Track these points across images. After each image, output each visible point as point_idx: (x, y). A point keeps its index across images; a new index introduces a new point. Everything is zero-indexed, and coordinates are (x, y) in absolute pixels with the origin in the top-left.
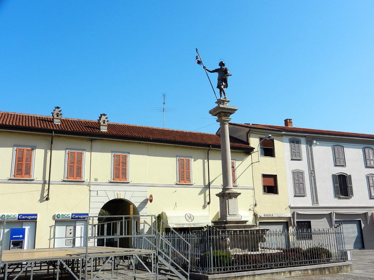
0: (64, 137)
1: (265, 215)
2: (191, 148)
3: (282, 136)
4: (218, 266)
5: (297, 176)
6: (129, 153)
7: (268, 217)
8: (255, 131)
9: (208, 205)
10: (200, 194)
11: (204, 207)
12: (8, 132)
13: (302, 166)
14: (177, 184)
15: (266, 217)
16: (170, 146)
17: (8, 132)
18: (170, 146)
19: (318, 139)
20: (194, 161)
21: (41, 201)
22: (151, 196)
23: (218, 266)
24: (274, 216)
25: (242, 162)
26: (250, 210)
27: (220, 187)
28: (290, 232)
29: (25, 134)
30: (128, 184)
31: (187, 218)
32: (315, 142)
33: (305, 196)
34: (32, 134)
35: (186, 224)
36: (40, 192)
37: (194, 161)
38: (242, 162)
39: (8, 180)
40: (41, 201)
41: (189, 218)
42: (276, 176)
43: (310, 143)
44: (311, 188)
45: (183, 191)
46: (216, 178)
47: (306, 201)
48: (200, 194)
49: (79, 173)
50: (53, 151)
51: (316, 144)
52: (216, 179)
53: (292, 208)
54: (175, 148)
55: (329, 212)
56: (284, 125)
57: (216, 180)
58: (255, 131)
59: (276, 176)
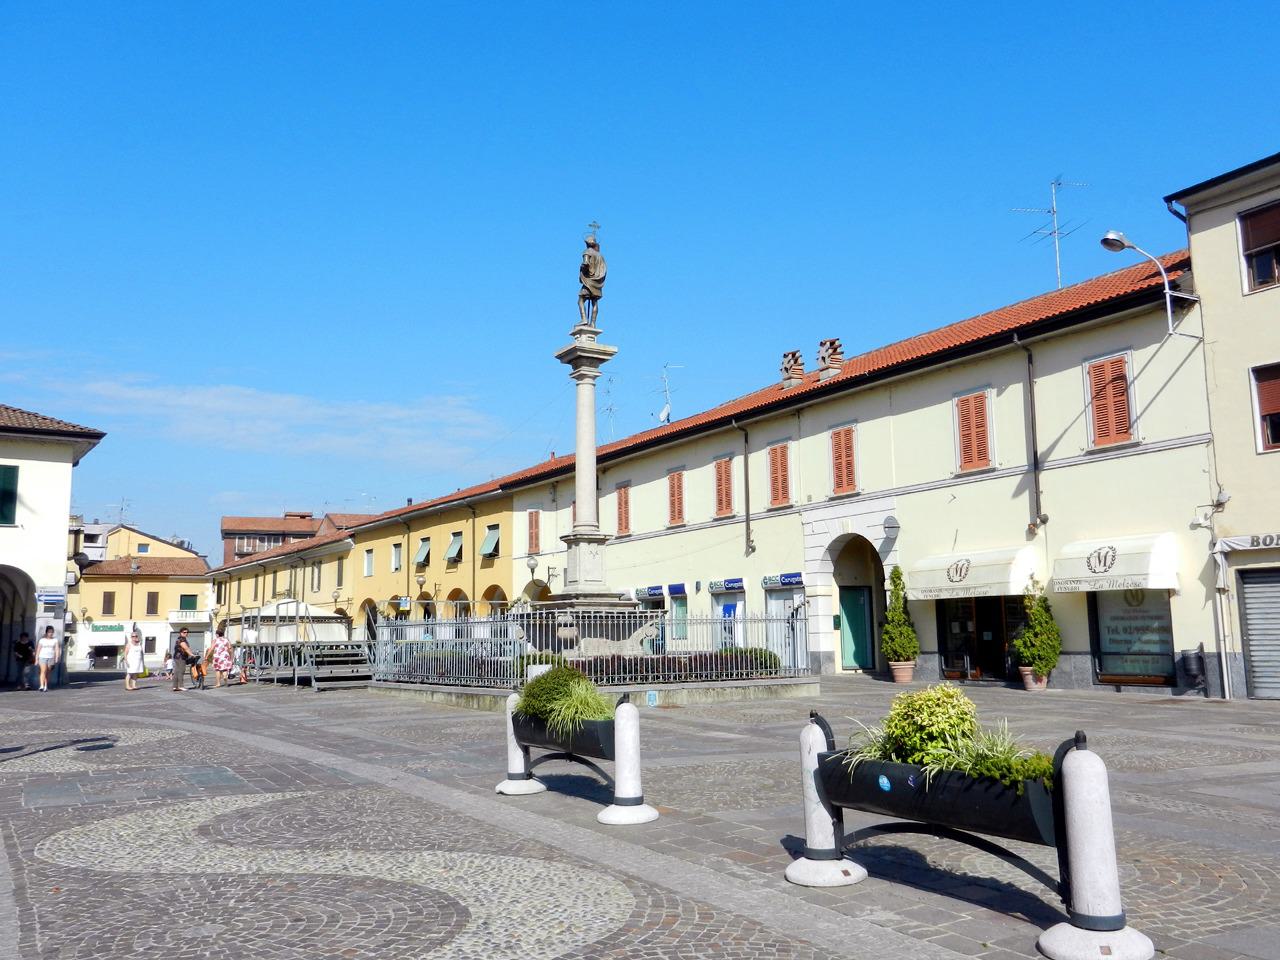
0: (714, 434)
2: (991, 357)
4: (630, 672)
6: (856, 421)
7: (1273, 546)
8: (1215, 197)
9: (1043, 526)
10: (1018, 493)
11: (1031, 532)
12: (940, 369)
14: (716, 520)
15: (1262, 546)
16: (932, 372)
17: (940, 369)
18: (932, 372)
20: (999, 394)
21: (748, 554)
23: (630, 672)
25: (1161, 347)
26: (1195, 526)
27: (1079, 458)
28: (689, 617)
29: (962, 364)
30: (1138, 449)
31: (1095, 561)
35: (946, 590)
36: (745, 536)
37: (999, 394)
38: (1161, 347)
39: (953, 478)
40: (748, 554)
41: (1100, 562)
42: (182, 596)
45: (974, 491)
46: (1066, 430)
48: (1018, 493)
49: (983, 454)
52: (1061, 436)
54: (950, 371)
57: (1065, 437)
58: (1215, 197)
59: (182, 596)
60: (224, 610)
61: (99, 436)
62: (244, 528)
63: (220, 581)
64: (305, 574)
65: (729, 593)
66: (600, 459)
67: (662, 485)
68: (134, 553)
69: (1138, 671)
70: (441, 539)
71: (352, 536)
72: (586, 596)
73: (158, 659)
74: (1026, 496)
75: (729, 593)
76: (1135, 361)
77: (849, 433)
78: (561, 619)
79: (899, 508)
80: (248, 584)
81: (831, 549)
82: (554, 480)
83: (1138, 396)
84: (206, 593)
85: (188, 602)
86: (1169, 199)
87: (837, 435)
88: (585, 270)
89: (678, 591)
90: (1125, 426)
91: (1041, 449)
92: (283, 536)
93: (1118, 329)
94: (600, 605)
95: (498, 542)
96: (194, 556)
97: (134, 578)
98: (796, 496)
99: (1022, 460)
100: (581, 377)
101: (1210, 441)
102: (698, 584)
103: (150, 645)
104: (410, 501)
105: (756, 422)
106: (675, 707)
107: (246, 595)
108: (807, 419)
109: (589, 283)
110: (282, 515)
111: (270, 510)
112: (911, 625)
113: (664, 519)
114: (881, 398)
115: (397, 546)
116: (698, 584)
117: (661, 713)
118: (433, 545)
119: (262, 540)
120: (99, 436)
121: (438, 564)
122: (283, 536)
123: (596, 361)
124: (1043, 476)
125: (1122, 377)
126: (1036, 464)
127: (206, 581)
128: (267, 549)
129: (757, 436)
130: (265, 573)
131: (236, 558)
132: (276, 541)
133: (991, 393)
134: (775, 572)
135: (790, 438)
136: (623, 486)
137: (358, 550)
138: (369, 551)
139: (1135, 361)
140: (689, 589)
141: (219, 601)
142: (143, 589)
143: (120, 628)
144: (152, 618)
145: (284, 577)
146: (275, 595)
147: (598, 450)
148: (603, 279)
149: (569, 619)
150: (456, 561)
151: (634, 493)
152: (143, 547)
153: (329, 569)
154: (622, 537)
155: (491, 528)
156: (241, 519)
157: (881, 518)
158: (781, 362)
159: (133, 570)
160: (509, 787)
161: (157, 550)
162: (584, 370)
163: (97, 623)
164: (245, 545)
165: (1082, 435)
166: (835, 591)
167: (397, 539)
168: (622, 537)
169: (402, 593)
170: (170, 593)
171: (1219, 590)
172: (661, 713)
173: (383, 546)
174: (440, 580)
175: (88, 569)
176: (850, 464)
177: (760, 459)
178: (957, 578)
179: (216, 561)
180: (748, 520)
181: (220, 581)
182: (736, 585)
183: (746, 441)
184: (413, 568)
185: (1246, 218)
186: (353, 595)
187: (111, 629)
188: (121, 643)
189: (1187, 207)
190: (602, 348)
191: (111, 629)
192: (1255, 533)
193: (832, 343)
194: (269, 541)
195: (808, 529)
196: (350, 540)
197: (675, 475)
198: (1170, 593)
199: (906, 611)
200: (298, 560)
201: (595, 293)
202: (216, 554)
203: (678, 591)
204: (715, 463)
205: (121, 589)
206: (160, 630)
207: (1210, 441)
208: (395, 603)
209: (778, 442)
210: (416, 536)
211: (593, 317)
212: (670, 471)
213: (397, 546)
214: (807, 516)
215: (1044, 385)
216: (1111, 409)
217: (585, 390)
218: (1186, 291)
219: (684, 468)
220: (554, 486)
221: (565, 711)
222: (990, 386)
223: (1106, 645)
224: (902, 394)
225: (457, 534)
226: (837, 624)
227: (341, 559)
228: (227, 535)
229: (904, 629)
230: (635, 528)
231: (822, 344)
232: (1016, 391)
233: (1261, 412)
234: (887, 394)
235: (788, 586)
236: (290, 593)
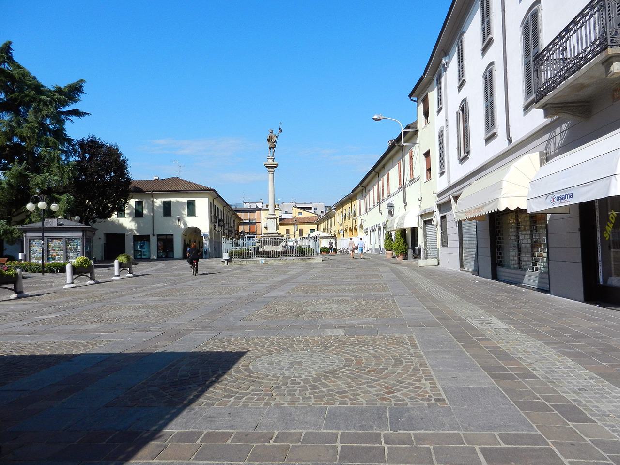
55: (446, 199)
88: (268, 140)
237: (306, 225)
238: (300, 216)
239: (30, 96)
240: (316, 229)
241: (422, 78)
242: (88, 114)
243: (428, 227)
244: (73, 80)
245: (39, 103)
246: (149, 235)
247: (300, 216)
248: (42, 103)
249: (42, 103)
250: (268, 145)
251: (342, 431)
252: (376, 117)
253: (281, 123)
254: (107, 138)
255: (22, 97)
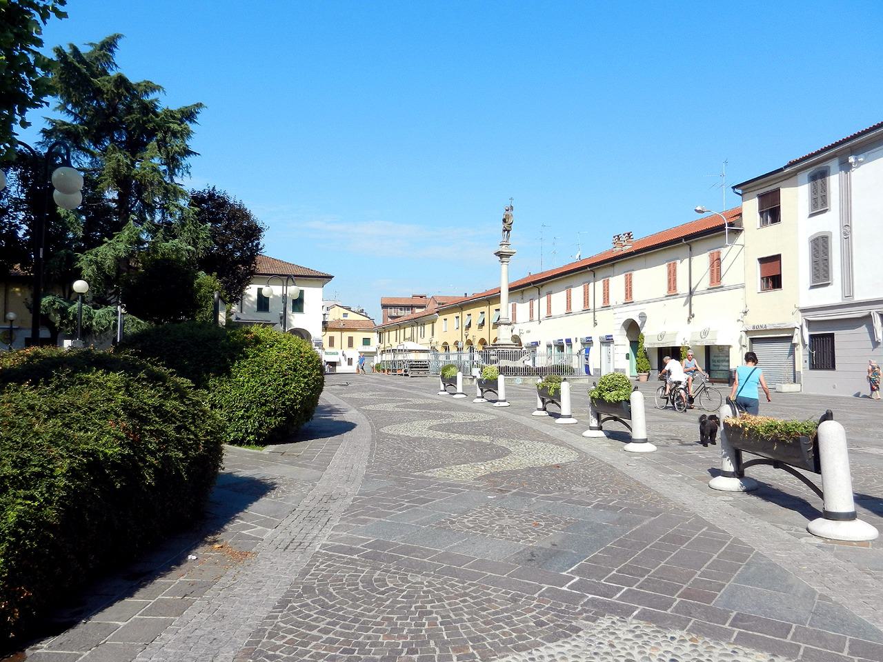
1: (754, 327)
3: (796, 175)
5: (820, 246)
10: (685, 305)
13: (828, 223)
19: (855, 151)
22: (29, 124)
24: (768, 328)
32: (852, 159)
33: (828, 284)
34: (673, 248)
43: (846, 167)
44: (843, 265)
47: (831, 295)
48: (685, 305)
50: (288, 287)
51: (859, 164)
53: (803, 311)
55: (865, 313)
56: (517, 304)
60: (382, 346)
61: (331, 277)
62: (392, 303)
63: (381, 331)
64: (417, 329)
65: (588, 343)
66: (510, 290)
67: (564, 294)
68: (342, 318)
69: (721, 377)
70: (476, 314)
71: (437, 312)
72: (502, 345)
73: (353, 369)
74: (688, 305)
75: (588, 343)
76: (724, 251)
77: (631, 275)
78: (492, 353)
79: (648, 309)
80: (393, 334)
81: (623, 325)
82: (491, 298)
83: (724, 266)
84: (374, 337)
85: (366, 342)
86: (734, 188)
87: (626, 275)
88: (504, 221)
89: (569, 341)
90: (719, 278)
91: (693, 287)
92: (411, 307)
93: (714, 240)
94: (507, 348)
95: (484, 320)
96: (368, 319)
97: (342, 330)
98: (612, 302)
99: (687, 291)
100: (503, 262)
101: (744, 287)
102: (576, 339)
103: (350, 362)
104: (466, 294)
105: (598, 268)
106: (527, 384)
107: (392, 339)
108: (617, 267)
109: (506, 225)
110: (411, 296)
111: (404, 293)
112: (647, 358)
113: (564, 310)
114: (642, 260)
115: (457, 317)
116: (576, 339)
117: (523, 386)
118: (472, 317)
119: (401, 309)
120: (331, 277)
121: (474, 327)
122: (411, 307)
123: (508, 256)
124: (694, 298)
125: (719, 259)
126: (691, 293)
127: (374, 332)
128: (406, 314)
129: (599, 274)
130: (400, 329)
131: (390, 320)
132: (408, 310)
133: (678, 262)
134: (604, 335)
135: (610, 276)
136: (549, 293)
137: (441, 318)
138: (445, 320)
139: (724, 251)
140: (573, 341)
141: (380, 342)
142: (346, 335)
143: (337, 354)
144: (350, 349)
145: (408, 330)
146: (405, 339)
147: (509, 286)
148: (512, 223)
149: (494, 353)
150: (482, 324)
151: (553, 296)
152: (345, 315)
153: (428, 327)
154: (627, 303)
155: (497, 310)
156: (391, 298)
157: (638, 313)
158: (611, 240)
159: (341, 326)
160: (441, 393)
161: (352, 316)
162: (504, 259)
163: (326, 351)
164: (393, 312)
165: (706, 283)
166: (628, 343)
167: (458, 314)
168: (627, 303)
169: (460, 340)
170: (358, 337)
171: (744, 346)
172: (523, 386)
173: (451, 317)
174: (476, 334)
175: (326, 326)
176: (630, 288)
177: (599, 284)
178: (704, 337)
179: (379, 322)
180: (594, 312)
181: (381, 331)
182: (590, 339)
183: (691, 250)
184: (464, 328)
185: (761, 197)
186: (439, 339)
187: (333, 354)
188: (337, 360)
189: (743, 190)
190: (510, 251)
191: (333, 354)
192: (754, 324)
193: (629, 234)
194: (405, 310)
195: (616, 316)
196: (437, 314)
197: (569, 288)
198: (729, 347)
199: (646, 353)
200: (417, 322)
201: (508, 229)
202: (378, 317)
203: (569, 341)
204: (624, 275)
205: (336, 335)
206: (354, 354)
207: (744, 287)
208: (456, 343)
209: (628, 272)
210: (465, 313)
211: (508, 237)
212: (567, 288)
213: (457, 317)
214: (616, 310)
215: (695, 259)
216: (715, 271)
217: (504, 267)
218: (738, 226)
219: (572, 287)
220: (522, 292)
221: (448, 374)
222: (678, 259)
223: (712, 368)
224: (650, 259)
225: (483, 313)
226: (628, 357)
227: (433, 323)
228: (384, 307)
229: (644, 359)
230: (553, 313)
231: (614, 237)
232: (687, 260)
233: (761, 274)
234: (644, 259)
235: (608, 341)
236: (412, 339)
237: (359, 331)
238: (345, 318)
239: (154, 122)
240: (596, 343)
241: (781, 170)
242: (195, 153)
243: (330, 326)
244: (187, 102)
245: (165, 133)
246: (813, 367)
247: (345, 318)
248: (169, 134)
249: (169, 134)
250: (501, 226)
251: (785, 640)
252: (698, 208)
253: (511, 199)
254: (235, 193)
255: (144, 121)
